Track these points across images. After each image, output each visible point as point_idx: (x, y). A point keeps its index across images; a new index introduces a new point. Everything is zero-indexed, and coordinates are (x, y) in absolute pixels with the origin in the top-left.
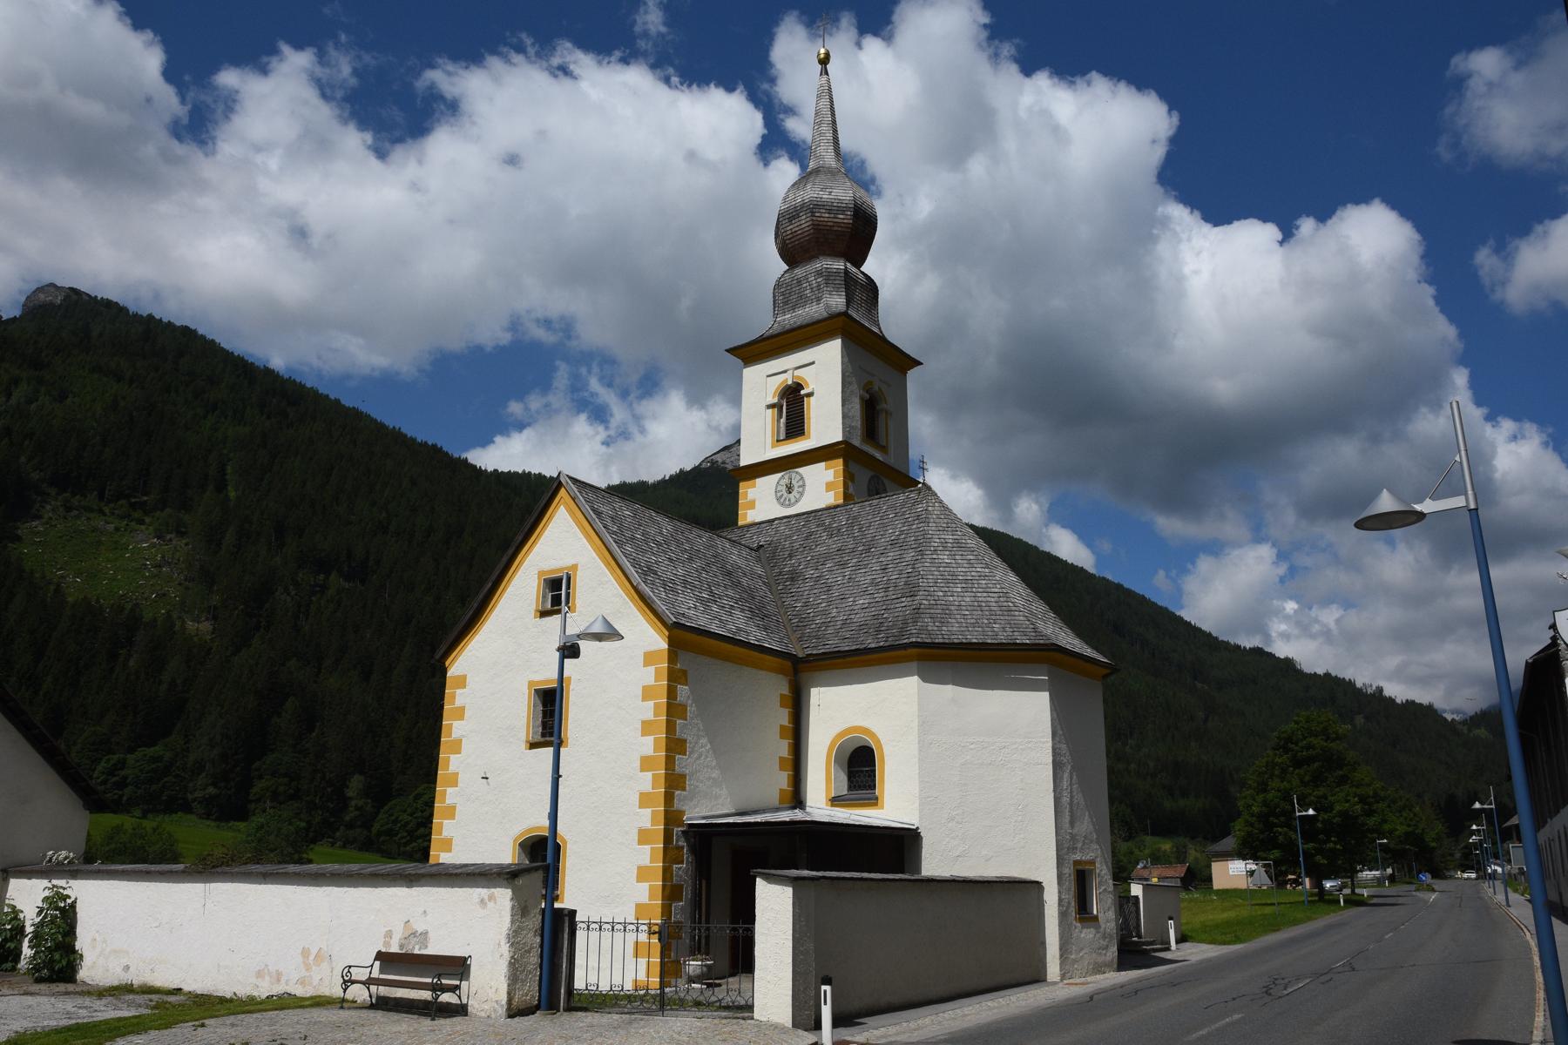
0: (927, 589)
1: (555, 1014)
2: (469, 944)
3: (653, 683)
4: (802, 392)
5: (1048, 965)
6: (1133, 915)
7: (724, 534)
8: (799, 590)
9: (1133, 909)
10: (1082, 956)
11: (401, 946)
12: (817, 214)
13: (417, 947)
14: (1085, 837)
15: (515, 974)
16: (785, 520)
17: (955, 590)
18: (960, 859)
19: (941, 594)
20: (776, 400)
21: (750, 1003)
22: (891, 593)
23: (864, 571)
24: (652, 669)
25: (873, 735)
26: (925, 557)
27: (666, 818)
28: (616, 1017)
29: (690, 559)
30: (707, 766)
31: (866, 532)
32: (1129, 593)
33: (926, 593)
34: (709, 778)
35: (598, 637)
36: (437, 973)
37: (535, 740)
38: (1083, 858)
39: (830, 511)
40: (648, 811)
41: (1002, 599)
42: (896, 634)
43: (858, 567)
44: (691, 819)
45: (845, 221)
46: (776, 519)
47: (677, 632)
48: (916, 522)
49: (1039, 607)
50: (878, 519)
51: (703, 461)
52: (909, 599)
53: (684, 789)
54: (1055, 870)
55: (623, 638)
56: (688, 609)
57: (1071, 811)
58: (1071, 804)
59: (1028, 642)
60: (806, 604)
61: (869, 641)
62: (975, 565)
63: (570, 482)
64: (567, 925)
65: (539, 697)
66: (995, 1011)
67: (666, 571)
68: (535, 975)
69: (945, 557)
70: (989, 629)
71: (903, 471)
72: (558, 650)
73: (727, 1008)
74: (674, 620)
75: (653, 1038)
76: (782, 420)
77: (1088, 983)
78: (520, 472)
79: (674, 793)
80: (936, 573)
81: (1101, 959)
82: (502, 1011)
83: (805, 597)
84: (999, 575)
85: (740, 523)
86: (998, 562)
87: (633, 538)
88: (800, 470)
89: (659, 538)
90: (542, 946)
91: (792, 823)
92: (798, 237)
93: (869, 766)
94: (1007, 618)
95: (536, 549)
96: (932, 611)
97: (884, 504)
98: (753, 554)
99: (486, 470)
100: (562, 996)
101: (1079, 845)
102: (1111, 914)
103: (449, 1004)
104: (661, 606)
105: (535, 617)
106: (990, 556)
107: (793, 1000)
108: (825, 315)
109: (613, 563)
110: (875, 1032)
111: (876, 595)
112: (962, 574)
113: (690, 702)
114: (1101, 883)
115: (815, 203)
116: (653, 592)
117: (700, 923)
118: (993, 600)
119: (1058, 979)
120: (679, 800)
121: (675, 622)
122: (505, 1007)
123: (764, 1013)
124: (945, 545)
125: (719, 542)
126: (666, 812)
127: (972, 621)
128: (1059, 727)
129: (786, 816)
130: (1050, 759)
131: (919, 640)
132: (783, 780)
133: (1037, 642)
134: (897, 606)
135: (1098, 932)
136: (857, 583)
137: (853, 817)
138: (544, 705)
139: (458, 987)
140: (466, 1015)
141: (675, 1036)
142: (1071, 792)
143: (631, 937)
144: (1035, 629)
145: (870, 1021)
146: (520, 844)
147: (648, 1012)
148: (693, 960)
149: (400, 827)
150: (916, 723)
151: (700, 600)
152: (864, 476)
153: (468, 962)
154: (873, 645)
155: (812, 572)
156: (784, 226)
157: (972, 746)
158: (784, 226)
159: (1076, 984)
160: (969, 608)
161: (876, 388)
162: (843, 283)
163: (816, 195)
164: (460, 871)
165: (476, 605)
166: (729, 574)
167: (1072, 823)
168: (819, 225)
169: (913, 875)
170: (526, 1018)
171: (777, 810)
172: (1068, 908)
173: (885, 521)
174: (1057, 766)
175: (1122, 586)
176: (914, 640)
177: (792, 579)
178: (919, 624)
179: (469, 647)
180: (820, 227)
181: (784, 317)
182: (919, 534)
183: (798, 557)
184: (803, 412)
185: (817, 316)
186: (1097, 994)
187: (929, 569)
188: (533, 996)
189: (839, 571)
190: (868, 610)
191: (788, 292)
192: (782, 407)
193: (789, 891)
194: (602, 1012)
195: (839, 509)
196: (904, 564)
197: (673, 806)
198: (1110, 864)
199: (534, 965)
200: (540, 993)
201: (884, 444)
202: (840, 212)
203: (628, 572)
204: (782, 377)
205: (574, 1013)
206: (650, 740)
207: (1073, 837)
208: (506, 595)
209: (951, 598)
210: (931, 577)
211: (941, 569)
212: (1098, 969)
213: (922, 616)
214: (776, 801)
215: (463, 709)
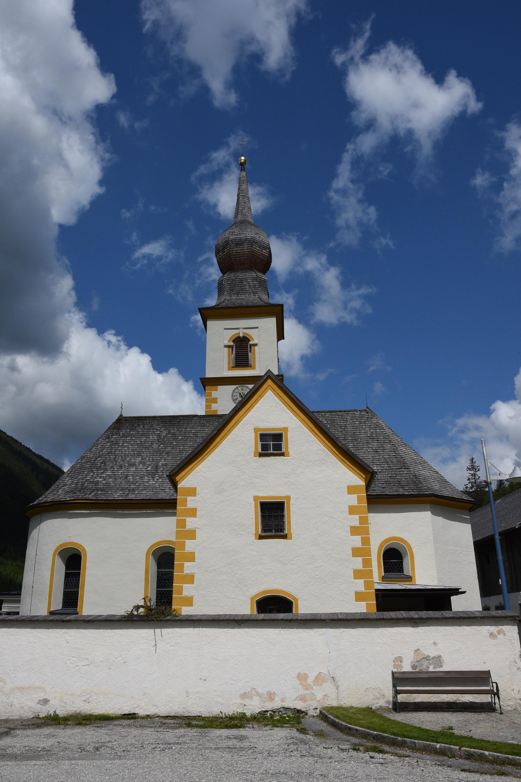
2: (485, 663)
11: (414, 667)
12: (254, 247)
45: (266, 254)
95: (251, 413)
157: (451, 552)
168: (254, 252)
204: (236, 331)
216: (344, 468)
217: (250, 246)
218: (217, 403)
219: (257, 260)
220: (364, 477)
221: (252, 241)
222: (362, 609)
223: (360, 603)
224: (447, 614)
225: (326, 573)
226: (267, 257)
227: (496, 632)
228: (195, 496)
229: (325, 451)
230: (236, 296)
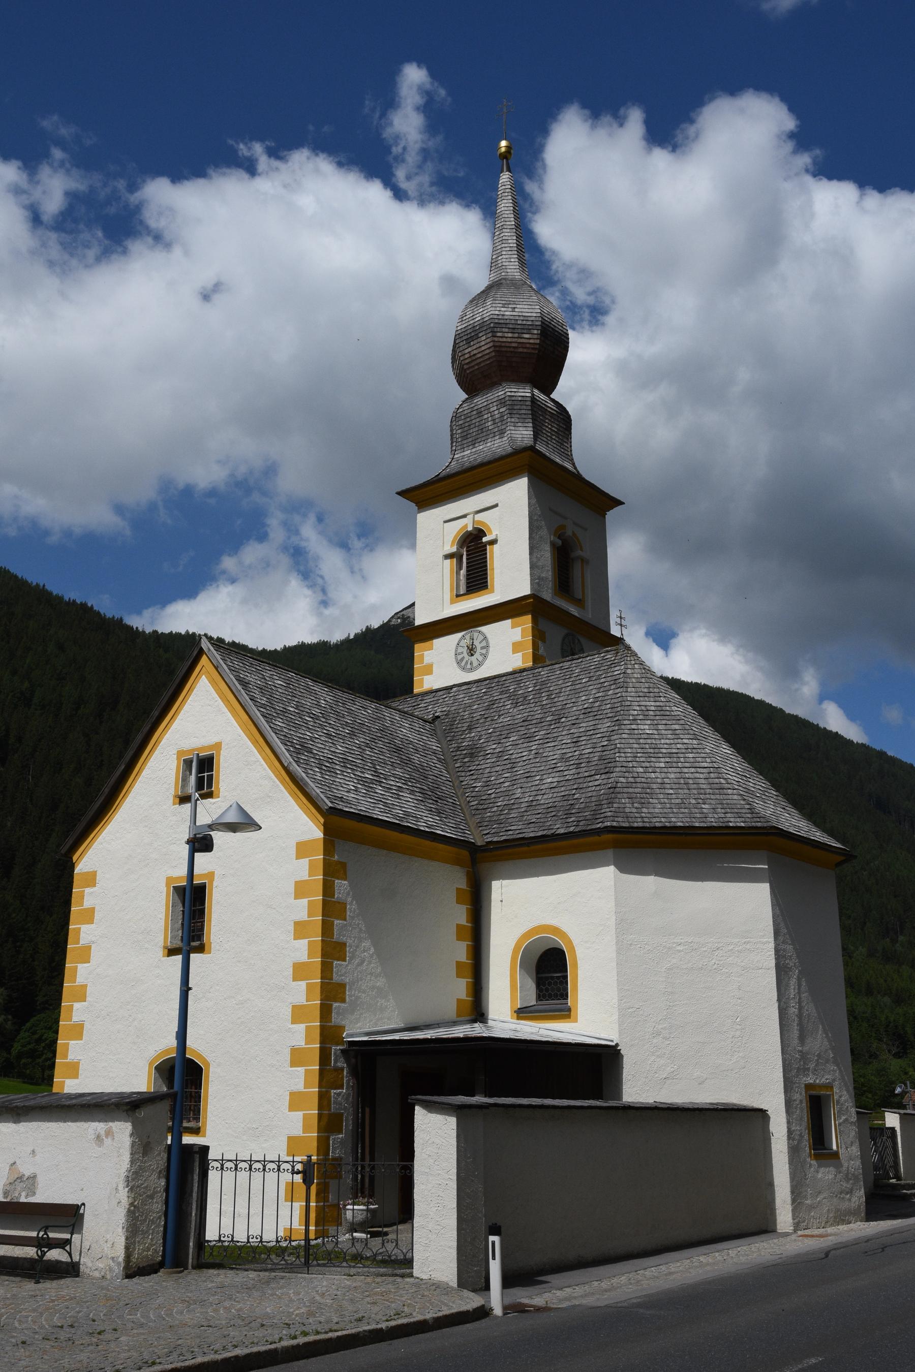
0: (625, 764)
1: (182, 1271)
2: (82, 1190)
3: (307, 878)
4: (485, 539)
5: (777, 1212)
6: (890, 1151)
7: (394, 705)
8: (479, 767)
9: (889, 1143)
10: (819, 1202)
11: (6, 1194)
12: (499, 334)
13: (23, 1194)
14: (819, 1056)
15: (135, 1224)
16: (464, 688)
17: (657, 765)
18: (668, 1082)
19: (641, 770)
20: (454, 549)
21: (409, 1255)
22: (584, 769)
23: (553, 744)
24: (305, 862)
25: (563, 935)
26: (623, 727)
27: (322, 1034)
28: (252, 1275)
29: (352, 734)
30: (371, 974)
31: (556, 700)
32: (893, 761)
33: (624, 769)
35: (233, 827)
36: (44, 1225)
37: (175, 946)
38: (818, 1081)
39: (516, 675)
40: (302, 1027)
41: (712, 775)
42: (588, 817)
43: (546, 740)
44: (352, 1035)
45: (531, 341)
46: (454, 686)
47: (336, 819)
48: (613, 687)
49: (758, 783)
50: (570, 683)
51: (393, 617)
52: (603, 776)
53: (344, 1001)
54: (782, 1096)
55: (261, 828)
56: (348, 792)
57: (800, 1024)
58: (800, 1016)
59: (743, 824)
60: (487, 784)
61: (557, 826)
62: (682, 736)
63: (212, 648)
64: (197, 1164)
66: (708, 1268)
67: (322, 747)
68: (158, 1226)
69: (646, 728)
70: (697, 811)
71: (604, 629)
72: (188, 842)
73: (385, 1263)
74: (330, 805)
75: (291, 1301)
76: (462, 572)
77: (827, 1235)
78: (183, 633)
79: (332, 1005)
80: (635, 746)
81: (844, 1206)
82: (118, 1270)
83: (486, 775)
84: (709, 747)
85: (416, 690)
86: (709, 732)
87: (285, 711)
88: (484, 629)
89: (316, 711)
90: (167, 1190)
91: (466, 1039)
92: (478, 361)
93: (561, 971)
94: (718, 797)
96: (631, 790)
97: (576, 666)
98: (428, 726)
99: (144, 632)
100: (191, 1251)
101: (812, 1066)
102: (855, 1150)
103: (58, 1262)
104: (315, 790)
105: (174, 804)
106: (700, 725)
107: (458, 1254)
108: (509, 450)
109: (261, 740)
110: (559, 1293)
111: (566, 773)
112: (666, 746)
113: (349, 899)
114: (840, 1112)
115: (496, 321)
116: (306, 773)
117: (363, 1159)
118: (701, 776)
119: (790, 1229)
121: (331, 808)
122: (123, 1265)
123: (425, 1269)
124: (646, 713)
125: (386, 713)
126: (323, 1028)
127: (677, 801)
128: (782, 925)
129: (460, 1031)
130: (773, 963)
131: (615, 824)
132: (461, 989)
133: (754, 824)
134: (590, 784)
135: (840, 1172)
136: (545, 759)
137: (542, 1032)
139: (68, 1242)
140: (77, 1275)
141: (318, 1298)
142: (800, 1002)
143: (286, 1177)
144: (752, 810)
145: (555, 1279)
147: (291, 1268)
149: (44, 1047)
150: (612, 922)
151: (362, 781)
152: (557, 634)
153: (81, 1211)
154: (562, 831)
155: (494, 746)
156: (461, 349)
157: (679, 948)
158: (461, 349)
159: (812, 1236)
160: (674, 786)
161: (569, 533)
163: (497, 313)
164: (74, 1101)
165: (107, 790)
166: (398, 750)
167: (802, 1039)
168: (500, 346)
169: (606, 1100)
170: (147, 1278)
171: (454, 1023)
172: (800, 1141)
173: (577, 687)
174: (781, 970)
175: (885, 753)
176: (609, 824)
177: (472, 755)
178: (615, 805)
179: (100, 839)
180: (503, 349)
181: (462, 454)
182: (616, 701)
183: (479, 729)
184: (486, 561)
185: (500, 452)
186: (835, 1249)
187: (627, 741)
188: (156, 1251)
189: (525, 745)
190: (556, 790)
191: (467, 424)
192: (462, 556)
193: (452, 1121)
194: (237, 1269)
195: (525, 674)
196: (599, 736)
197: (331, 1022)
198: (851, 1088)
199: (158, 1212)
200: (164, 1246)
201: (581, 597)
202: (525, 331)
203: (278, 751)
205: (205, 1270)
206: (303, 944)
207: (804, 1056)
209: (653, 775)
210: (629, 750)
211: (641, 741)
212: (841, 1218)
213: (619, 796)
214: (451, 1011)
215: (92, 910)
216: (297, 807)
217: (490, 335)
218: (432, 674)
222: (297, 1080)
223: (296, 1070)
224: (40, 1099)
226: (538, 346)
227: (104, 1132)
228: (95, 886)
229: (270, 778)
230: (471, 447)
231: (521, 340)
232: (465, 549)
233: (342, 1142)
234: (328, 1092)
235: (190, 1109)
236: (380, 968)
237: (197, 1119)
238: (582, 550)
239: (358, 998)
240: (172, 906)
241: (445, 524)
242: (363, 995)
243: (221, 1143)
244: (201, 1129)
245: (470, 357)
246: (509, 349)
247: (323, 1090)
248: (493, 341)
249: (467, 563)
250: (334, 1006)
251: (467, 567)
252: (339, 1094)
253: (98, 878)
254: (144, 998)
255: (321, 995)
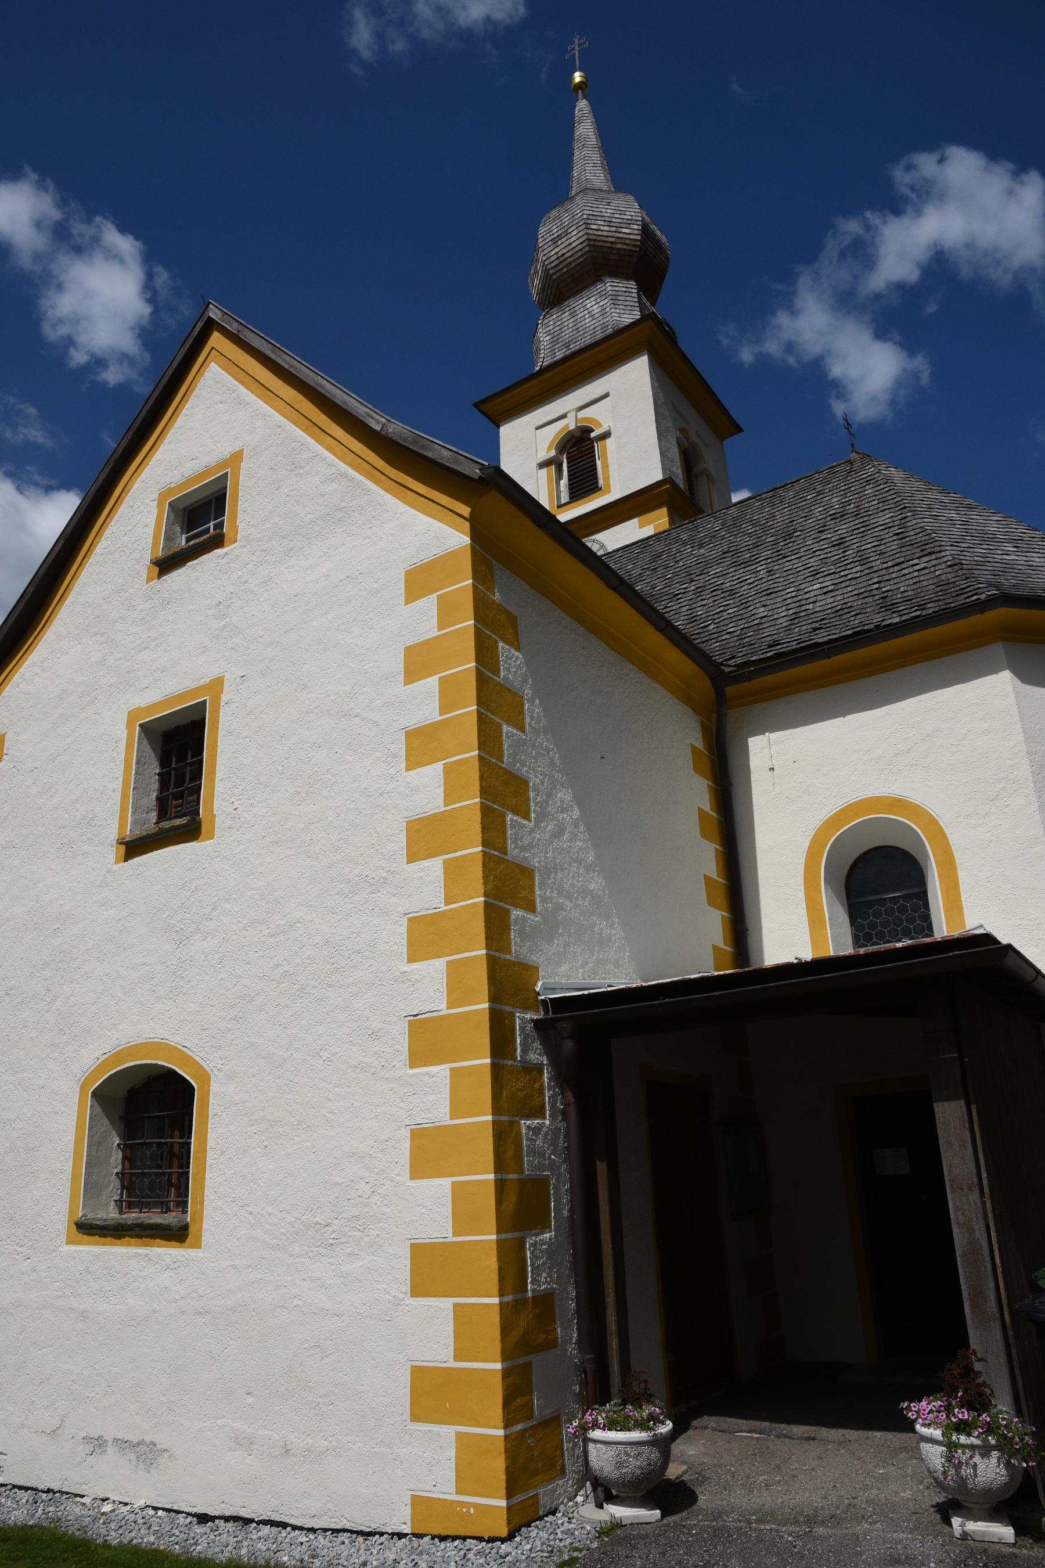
4: (593, 435)
12: (593, 227)
20: (553, 453)
30: (579, 861)
34: (585, 892)
45: (632, 237)
53: (531, 908)
65: (151, 742)
76: (562, 482)
79: (507, 912)
92: (568, 261)
120: (521, 933)
126: (493, 963)
138: (164, 762)
146: (95, 1094)
148: (611, 1425)
162: (637, 304)
168: (595, 240)
180: (599, 244)
191: (557, 329)
197: (510, 953)
206: (432, 775)
208: (92, 559)
219: (611, 257)
220: (467, 515)
221: (585, 216)
222: (433, 1097)
225: (308, 953)
226: (639, 243)
229: (345, 475)
231: (620, 235)
232: (565, 456)
233: (552, 1251)
234: (513, 1125)
235: (170, 1184)
236: (592, 853)
237: (183, 1205)
238: (705, 463)
239: (558, 907)
240: (137, 763)
241: (537, 431)
242: (567, 903)
243: (237, 1263)
244: (191, 1229)
245: (558, 258)
246: (605, 244)
247: (504, 1118)
248: (587, 234)
249: (569, 471)
250: (513, 917)
251: (569, 476)
252: (537, 1130)
253: (6, 745)
254: (75, 951)
255: (485, 884)
